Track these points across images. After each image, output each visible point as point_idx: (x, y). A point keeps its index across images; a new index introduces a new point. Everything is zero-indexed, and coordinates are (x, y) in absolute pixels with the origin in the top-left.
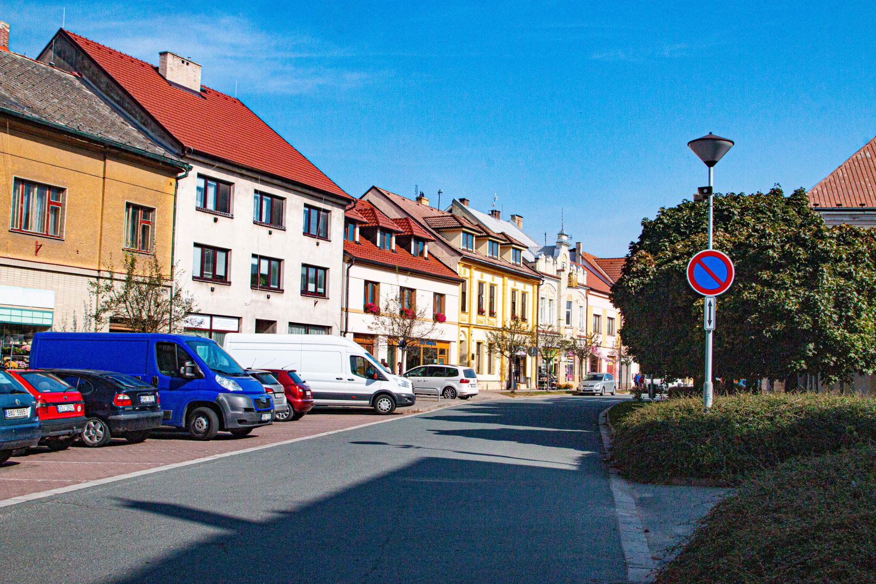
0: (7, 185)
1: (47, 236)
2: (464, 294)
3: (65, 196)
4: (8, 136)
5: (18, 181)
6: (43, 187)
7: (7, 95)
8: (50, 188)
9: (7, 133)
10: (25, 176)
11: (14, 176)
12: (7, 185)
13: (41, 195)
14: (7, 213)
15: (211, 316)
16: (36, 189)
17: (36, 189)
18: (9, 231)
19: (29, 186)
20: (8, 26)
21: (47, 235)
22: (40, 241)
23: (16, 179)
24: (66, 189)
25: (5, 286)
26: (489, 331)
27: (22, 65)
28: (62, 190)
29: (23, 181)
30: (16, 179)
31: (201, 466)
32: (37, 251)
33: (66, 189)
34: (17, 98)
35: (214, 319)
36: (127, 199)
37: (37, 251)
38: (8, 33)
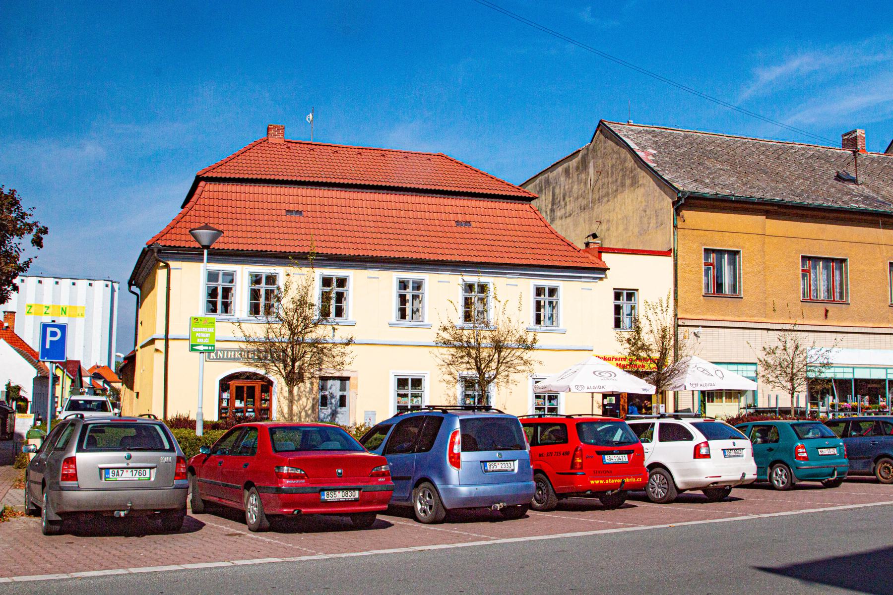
0: (884, 270)
1: (833, 302)
2: (676, 265)
3: (740, 257)
4: (881, 230)
5: (804, 258)
6: (827, 260)
7: (875, 195)
8: (833, 260)
9: (673, 207)
10: (721, 246)
11: (888, 262)
12: (884, 270)
13: (826, 268)
14: (886, 292)
15: (886, 369)
16: (821, 263)
17: (821, 263)
18: (703, 296)
19: (815, 261)
20: (863, 132)
21: (834, 300)
22: (829, 307)
23: (803, 257)
24: (846, 259)
25: (889, 351)
26: (614, 362)
27: (879, 163)
28: (844, 261)
29: (809, 258)
30: (803, 257)
31: (775, 518)
32: (826, 316)
33: (846, 259)
34: (883, 197)
35: (888, 370)
36: (889, 259)
37: (826, 316)
38: (864, 138)
